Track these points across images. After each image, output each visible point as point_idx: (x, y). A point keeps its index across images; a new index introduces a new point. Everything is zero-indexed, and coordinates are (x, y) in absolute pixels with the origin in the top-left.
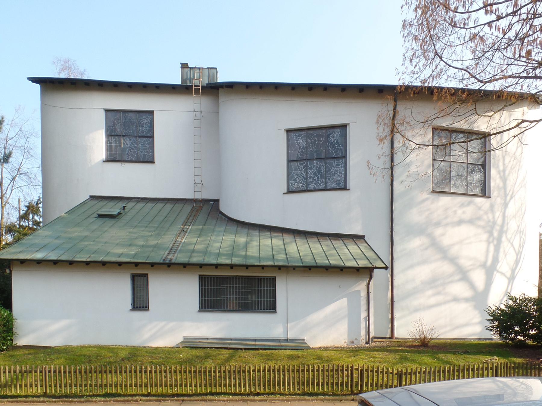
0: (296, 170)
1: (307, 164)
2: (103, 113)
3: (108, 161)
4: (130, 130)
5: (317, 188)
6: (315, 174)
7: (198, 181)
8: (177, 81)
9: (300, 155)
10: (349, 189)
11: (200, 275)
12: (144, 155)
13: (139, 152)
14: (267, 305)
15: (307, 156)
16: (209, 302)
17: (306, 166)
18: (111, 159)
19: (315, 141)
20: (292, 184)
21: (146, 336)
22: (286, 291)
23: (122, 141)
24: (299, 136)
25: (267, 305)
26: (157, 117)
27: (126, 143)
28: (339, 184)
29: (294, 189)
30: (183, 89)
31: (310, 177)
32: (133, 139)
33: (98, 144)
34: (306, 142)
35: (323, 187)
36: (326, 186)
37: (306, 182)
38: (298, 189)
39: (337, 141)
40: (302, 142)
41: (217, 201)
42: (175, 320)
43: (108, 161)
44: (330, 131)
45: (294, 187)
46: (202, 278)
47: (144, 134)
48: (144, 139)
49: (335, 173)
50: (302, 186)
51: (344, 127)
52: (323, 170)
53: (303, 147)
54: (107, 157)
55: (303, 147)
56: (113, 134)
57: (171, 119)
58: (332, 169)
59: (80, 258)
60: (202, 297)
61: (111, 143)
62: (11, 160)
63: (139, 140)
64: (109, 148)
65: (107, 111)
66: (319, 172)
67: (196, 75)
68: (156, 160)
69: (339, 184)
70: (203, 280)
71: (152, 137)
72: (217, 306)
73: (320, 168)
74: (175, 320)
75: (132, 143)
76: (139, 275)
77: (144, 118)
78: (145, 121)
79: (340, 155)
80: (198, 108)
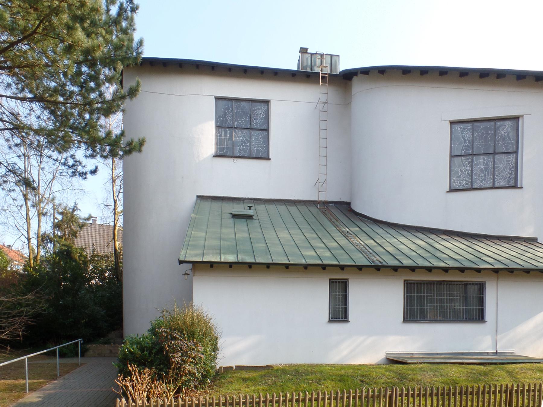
0: (460, 166)
1: (472, 159)
2: (213, 101)
3: (216, 156)
4: (242, 122)
5: (484, 186)
6: (481, 171)
7: (322, 180)
8: (293, 66)
9: (466, 149)
10: (521, 188)
11: (404, 281)
12: (257, 150)
13: (253, 147)
14: (478, 315)
15: (473, 151)
16: (413, 313)
17: (472, 161)
18: (219, 155)
19: (483, 134)
20: (454, 181)
21: (345, 353)
22: (498, 298)
23: (234, 134)
24: (464, 129)
25: (478, 315)
26: (273, 107)
27: (238, 136)
28: (509, 182)
29: (457, 187)
30: (303, 76)
31: (476, 174)
32: (245, 132)
33: (207, 136)
34: (473, 134)
35: (491, 185)
36: (494, 184)
37: (472, 179)
38: (461, 187)
39: (508, 134)
40: (468, 135)
41: (349, 204)
42: (378, 333)
43: (216, 156)
44: (499, 123)
45: (455, 186)
46: (407, 284)
47: (258, 127)
48: (258, 132)
49: (504, 170)
50: (467, 184)
51: (516, 119)
52: (491, 166)
53: (469, 141)
54: (216, 152)
55: (469, 141)
56: (224, 125)
57: (291, 111)
58: (501, 166)
59: (281, 260)
60: (407, 305)
61: (220, 136)
62: (144, 148)
63: (253, 132)
64: (219, 142)
65: (217, 99)
66: (486, 169)
67: (318, 62)
68: (271, 156)
69: (509, 182)
70: (408, 286)
71: (267, 130)
72: (424, 316)
73: (487, 164)
74: (378, 333)
75: (244, 136)
76: (339, 282)
77: (259, 109)
78: (259, 112)
79: (511, 150)
80: (323, 98)
